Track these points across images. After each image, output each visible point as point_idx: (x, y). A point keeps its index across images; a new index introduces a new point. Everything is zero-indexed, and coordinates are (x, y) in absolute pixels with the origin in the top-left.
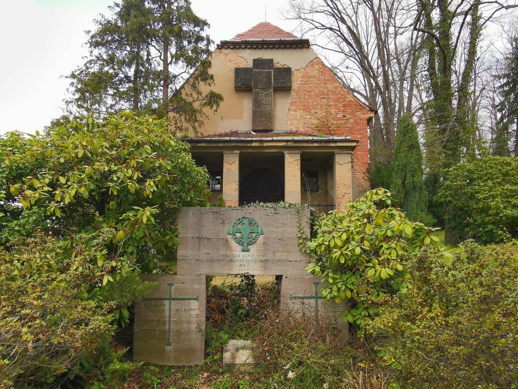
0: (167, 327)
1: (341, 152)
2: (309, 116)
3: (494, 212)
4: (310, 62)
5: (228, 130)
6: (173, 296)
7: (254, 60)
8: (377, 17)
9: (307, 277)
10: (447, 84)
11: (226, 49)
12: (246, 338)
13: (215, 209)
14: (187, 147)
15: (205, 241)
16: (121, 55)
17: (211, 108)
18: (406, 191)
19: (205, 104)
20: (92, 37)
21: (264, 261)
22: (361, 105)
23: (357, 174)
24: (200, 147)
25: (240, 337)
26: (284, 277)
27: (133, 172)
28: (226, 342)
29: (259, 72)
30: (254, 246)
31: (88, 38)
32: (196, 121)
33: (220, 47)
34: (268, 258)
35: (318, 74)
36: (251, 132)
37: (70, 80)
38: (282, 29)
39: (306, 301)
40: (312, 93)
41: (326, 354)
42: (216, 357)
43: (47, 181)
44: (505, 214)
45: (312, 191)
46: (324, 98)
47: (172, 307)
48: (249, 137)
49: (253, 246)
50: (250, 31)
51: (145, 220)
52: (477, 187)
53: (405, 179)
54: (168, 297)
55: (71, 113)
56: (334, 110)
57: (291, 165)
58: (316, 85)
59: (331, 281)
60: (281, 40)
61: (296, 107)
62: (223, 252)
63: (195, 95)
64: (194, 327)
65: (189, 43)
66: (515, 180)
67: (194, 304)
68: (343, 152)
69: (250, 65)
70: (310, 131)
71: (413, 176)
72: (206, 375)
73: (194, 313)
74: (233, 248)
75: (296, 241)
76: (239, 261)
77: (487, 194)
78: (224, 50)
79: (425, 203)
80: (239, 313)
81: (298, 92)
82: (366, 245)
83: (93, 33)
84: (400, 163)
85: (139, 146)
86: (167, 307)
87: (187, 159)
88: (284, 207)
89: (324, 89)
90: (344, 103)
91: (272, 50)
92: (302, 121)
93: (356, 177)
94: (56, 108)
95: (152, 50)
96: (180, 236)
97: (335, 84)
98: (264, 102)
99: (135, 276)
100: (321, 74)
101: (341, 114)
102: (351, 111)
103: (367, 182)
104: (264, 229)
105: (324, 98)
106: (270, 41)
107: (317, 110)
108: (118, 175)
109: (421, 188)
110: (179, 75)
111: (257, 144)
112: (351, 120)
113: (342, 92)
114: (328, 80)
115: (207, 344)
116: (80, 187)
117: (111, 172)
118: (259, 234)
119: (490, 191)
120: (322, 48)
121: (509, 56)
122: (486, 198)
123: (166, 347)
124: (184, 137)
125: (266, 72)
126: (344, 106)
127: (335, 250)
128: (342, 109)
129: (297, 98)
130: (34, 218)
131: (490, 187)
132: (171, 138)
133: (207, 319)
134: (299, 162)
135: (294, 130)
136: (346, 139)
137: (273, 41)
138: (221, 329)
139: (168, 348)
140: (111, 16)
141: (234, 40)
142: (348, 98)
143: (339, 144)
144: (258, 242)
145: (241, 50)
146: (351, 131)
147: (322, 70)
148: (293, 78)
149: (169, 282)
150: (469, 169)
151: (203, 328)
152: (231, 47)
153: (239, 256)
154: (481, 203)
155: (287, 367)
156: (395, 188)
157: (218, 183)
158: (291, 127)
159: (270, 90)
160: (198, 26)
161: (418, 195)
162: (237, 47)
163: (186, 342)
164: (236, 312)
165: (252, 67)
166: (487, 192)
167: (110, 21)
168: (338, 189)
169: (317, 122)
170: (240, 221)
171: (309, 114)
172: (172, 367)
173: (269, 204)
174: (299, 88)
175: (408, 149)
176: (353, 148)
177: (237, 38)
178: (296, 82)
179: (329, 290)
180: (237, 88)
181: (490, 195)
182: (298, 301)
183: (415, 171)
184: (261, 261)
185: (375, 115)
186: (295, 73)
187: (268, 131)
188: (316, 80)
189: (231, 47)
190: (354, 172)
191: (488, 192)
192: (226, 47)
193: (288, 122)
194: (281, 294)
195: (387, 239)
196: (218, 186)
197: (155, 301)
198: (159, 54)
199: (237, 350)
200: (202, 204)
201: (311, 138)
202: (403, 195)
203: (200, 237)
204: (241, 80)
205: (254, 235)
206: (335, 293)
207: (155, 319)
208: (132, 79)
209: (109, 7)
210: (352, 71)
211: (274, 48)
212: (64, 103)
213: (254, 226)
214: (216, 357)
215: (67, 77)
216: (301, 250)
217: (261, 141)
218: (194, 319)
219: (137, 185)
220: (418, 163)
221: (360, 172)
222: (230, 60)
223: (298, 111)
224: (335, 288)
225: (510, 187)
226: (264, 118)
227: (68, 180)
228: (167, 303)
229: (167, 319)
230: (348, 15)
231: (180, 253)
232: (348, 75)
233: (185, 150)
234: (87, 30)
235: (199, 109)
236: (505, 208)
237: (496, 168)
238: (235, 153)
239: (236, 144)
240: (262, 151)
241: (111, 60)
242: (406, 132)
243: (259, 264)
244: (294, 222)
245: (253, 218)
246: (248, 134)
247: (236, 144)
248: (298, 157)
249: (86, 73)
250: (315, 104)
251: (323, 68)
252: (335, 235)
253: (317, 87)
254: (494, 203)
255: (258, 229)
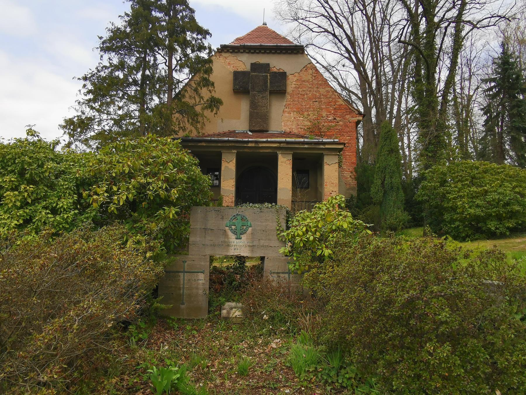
0: (182, 292)
1: (329, 153)
2: (302, 119)
3: (461, 210)
4: (304, 67)
5: (226, 130)
6: (186, 270)
7: (252, 64)
8: (372, 20)
9: (282, 258)
10: (432, 91)
11: (225, 52)
12: (238, 301)
13: (217, 208)
14: (196, 162)
15: (210, 231)
16: (131, 61)
17: (212, 111)
18: (385, 191)
19: (206, 108)
20: (103, 43)
21: (251, 246)
22: (350, 109)
23: (345, 173)
24: (200, 146)
25: (234, 301)
26: (266, 258)
27: (162, 183)
28: (223, 304)
29: (256, 76)
30: (245, 235)
31: (98, 43)
32: (198, 122)
33: (220, 51)
34: (254, 244)
35: (311, 79)
36: (248, 132)
37: (83, 82)
38: (279, 34)
39: (282, 275)
40: (306, 96)
41: (337, 374)
42: (216, 313)
43: (105, 189)
44: (469, 212)
45: (302, 188)
46: (316, 101)
47: (185, 278)
48: (246, 138)
49: (244, 235)
50: (248, 35)
51: (171, 216)
52: (448, 188)
53: (384, 180)
54: (182, 270)
55: (84, 114)
56: (326, 113)
57: (284, 164)
58: (309, 89)
59: (295, 259)
60: (277, 46)
61: (290, 109)
62: (222, 239)
63: (198, 100)
64: (201, 292)
65: (193, 51)
66: (480, 183)
67: (201, 276)
68: (331, 153)
69: (248, 68)
70: (302, 132)
71: (391, 178)
72: (209, 324)
73: (201, 282)
74: (230, 237)
75: (275, 233)
76: (233, 246)
77: (456, 194)
78: (223, 54)
79: (402, 201)
80: (233, 284)
81: (292, 95)
82: (318, 235)
83: (104, 39)
84: (381, 165)
85: (164, 164)
86: (182, 278)
87: (197, 172)
88: (268, 208)
89: (317, 92)
90: (335, 107)
91: (269, 55)
92: (295, 123)
93: (344, 176)
94: (69, 108)
95: (158, 57)
96: (191, 227)
97: (327, 89)
98: (260, 104)
99: (164, 254)
100: (314, 78)
101: (332, 117)
102: (341, 114)
103: (354, 181)
104: (252, 223)
105: (316, 101)
106: (267, 46)
107: (309, 113)
108: (153, 186)
109: (398, 188)
110: (183, 81)
111: (253, 145)
112: (341, 123)
113: (333, 97)
114: (321, 85)
115: (210, 304)
116: (129, 194)
117: (149, 184)
118: (248, 227)
119: (459, 192)
120: (319, 48)
121: (496, 61)
122: (455, 198)
123: (181, 305)
124: (186, 137)
125: (263, 76)
126: (335, 109)
127: (297, 238)
128: (332, 112)
129: (292, 100)
130: (94, 213)
131: (459, 189)
132: (185, 156)
133: (210, 288)
134: (291, 161)
135: (288, 130)
136: (334, 141)
137: (270, 46)
138: (220, 295)
139: (182, 306)
140: (120, 24)
141: (233, 44)
142: (339, 102)
143: (327, 146)
144: (248, 232)
145: (240, 54)
146: (341, 133)
147: (315, 75)
148: (288, 82)
149: (183, 260)
150: (442, 172)
151: (208, 292)
152: (230, 51)
153: (234, 242)
154: (451, 202)
155: (263, 313)
156: (375, 188)
157: (217, 179)
158: (285, 128)
159: (266, 92)
160: (201, 35)
161: (395, 194)
162: (236, 51)
163: (195, 303)
164: (231, 283)
165: (250, 71)
166: (456, 193)
167: (120, 28)
168: (326, 187)
169: (309, 124)
170: (235, 217)
171: (302, 116)
172: (186, 320)
173: (256, 205)
174: (293, 91)
175: (388, 153)
176: (340, 150)
177: (236, 42)
178: (291, 85)
179: (294, 265)
180: (235, 91)
181: (458, 196)
182: (275, 275)
183: (394, 172)
184: (249, 246)
185: (363, 118)
186: (290, 77)
187: (263, 131)
188: (310, 85)
189: (230, 51)
190: (343, 171)
191: (458, 193)
192: (226, 51)
193: (283, 123)
194: (264, 270)
195: (333, 231)
196: (216, 182)
197: (173, 273)
198: (165, 61)
199: (231, 309)
200: (206, 204)
201: (302, 140)
202: (381, 194)
203: (206, 228)
204: (240, 83)
205: (245, 227)
206: (297, 267)
207: (173, 286)
208: (140, 82)
209: (119, 16)
210: (348, 69)
211: (270, 53)
212: (77, 104)
213: (245, 221)
214: (216, 313)
215: (79, 79)
216: (278, 239)
217: (256, 142)
218: (201, 286)
219: (165, 192)
220: (396, 165)
221: (348, 171)
222: (229, 64)
223: (292, 113)
224: (297, 264)
225: (475, 189)
226: (260, 119)
227: (119, 189)
228: (181, 275)
229: (182, 286)
230: (344, 17)
231: (192, 239)
232: (343, 74)
233: (195, 164)
234: (100, 36)
235: (201, 112)
236: (470, 207)
237: (466, 172)
238: (233, 153)
239: (233, 144)
240: (257, 151)
241: (121, 66)
242: (387, 137)
243: (248, 248)
244: (274, 218)
245: (244, 215)
246: (244, 134)
247: (233, 144)
248: (290, 157)
249: (97, 77)
250: (308, 106)
251: (316, 73)
252: (298, 228)
253: (310, 91)
254: (461, 203)
255: (248, 223)
